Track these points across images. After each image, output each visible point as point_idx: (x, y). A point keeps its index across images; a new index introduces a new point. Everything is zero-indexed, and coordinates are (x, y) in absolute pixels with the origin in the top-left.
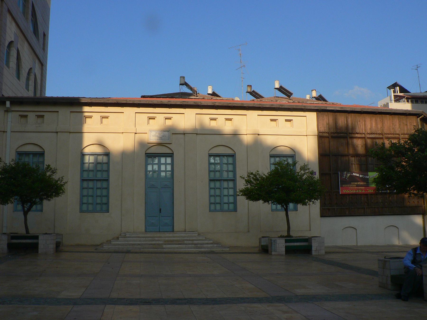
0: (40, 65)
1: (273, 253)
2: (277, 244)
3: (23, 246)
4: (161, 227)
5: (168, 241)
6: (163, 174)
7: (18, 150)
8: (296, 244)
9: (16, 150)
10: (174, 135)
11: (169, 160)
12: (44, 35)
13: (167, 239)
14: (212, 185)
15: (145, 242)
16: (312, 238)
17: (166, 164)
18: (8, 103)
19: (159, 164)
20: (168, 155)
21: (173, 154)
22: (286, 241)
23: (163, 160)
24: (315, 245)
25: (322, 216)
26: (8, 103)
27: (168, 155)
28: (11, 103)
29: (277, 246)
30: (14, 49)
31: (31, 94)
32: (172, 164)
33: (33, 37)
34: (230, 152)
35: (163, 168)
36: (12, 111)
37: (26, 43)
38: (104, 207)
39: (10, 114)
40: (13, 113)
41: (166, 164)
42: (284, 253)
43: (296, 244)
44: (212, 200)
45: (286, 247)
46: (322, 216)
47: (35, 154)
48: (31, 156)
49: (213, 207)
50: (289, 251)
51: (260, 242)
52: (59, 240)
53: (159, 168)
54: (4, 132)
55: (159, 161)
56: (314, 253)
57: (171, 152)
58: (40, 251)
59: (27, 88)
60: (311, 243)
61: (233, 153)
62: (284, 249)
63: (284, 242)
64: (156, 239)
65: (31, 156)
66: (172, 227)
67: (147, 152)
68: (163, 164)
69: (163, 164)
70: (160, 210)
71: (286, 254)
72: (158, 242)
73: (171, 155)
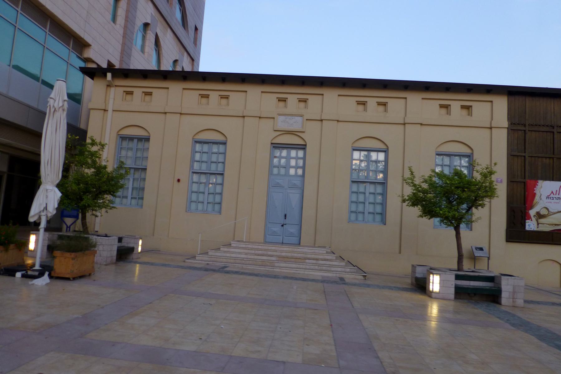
0: (191, 61)
4: (267, 236)
5: (284, 257)
6: (292, 172)
7: (121, 133)
9: (118, 132)
10: (308, 122)
11: (301, 153)
12: (196, 29)
13: (284, 254)
14: (355, 188)
15: (289, 255)
16: (503, 277)
17: (297, 158)
19: (288, 158)
20: (298, 147)
21: (306, 145)
22: (458, 277)
23: (293, 153)
24: (506, 286)
25: (507, 241)
26: (109, 75)
27: (298, 147)
28: (113, 77)
30: (151, 33)
32: (304, 158)
33: (181, 29)
34: (220, 138)
35: (293, 162)
36: (116, 86)
37: (169, 30)
38: (217, 207)
39: (113, 89)
40: (117, 88)
41: (297, 158)
42: (452, 296)
44: (353, 208)
46: (507, 241)
49: (353, 216)
51: (414, 271)
53: (288, 162)
55: (289, 154)
56: (504, 301)
57: (303, 143)
60: (500, 284)
65: (136, 141)
66: (299, 238)
67: (273, 142)
68: (293, 158)
69: (293, 158)
70: (285, 216)
71: (456, 298)
73: (303, 147)
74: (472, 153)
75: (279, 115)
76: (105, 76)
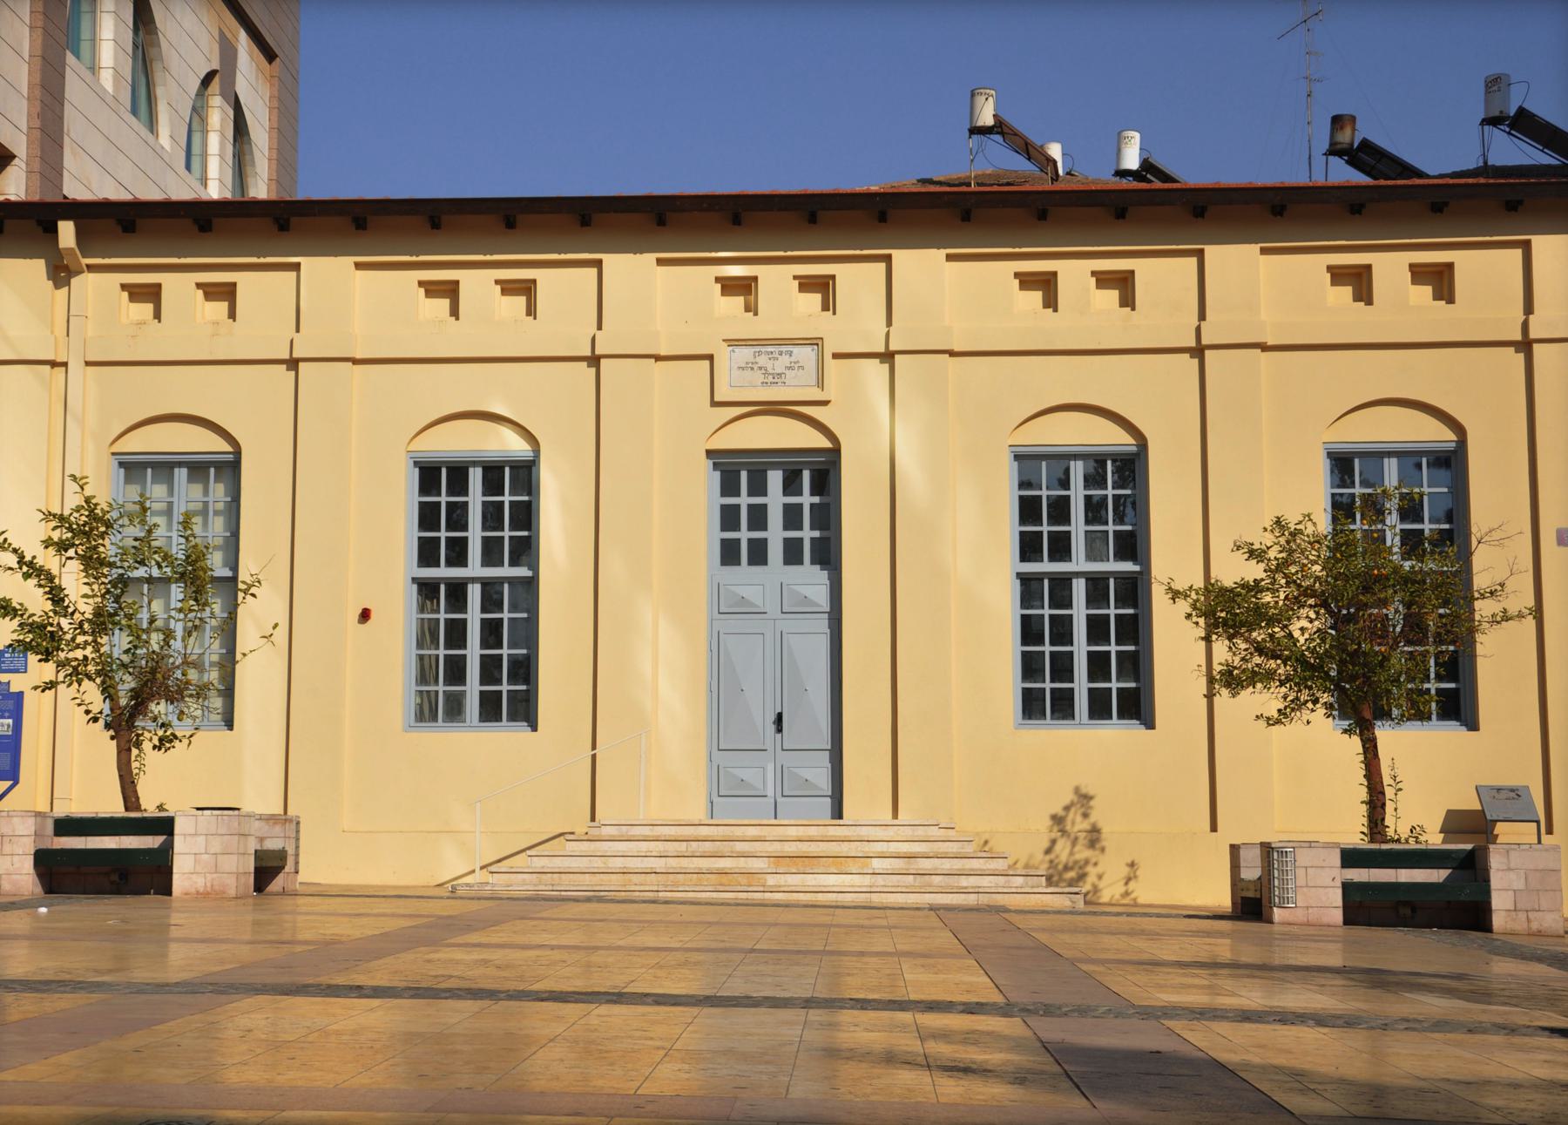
1: (1278, 914)
2: (1300, 872)
3: (107, 865)
4: (780, 800)
8: (1405, 876)
18: (67, 232)
26: (67, 232)
29: (1301, 881)
31: (216, 189)
43: (1405, 876)
45: (1348, 887)
47: (198, 468)
48: (181, 474)
50: (1362, 907)
52: (273, 845)
54: (53, 364)
56: (1498, 921)
58: (179, 883)
59: (192, 156)
61: (1448, 435)
62: (1337, 897)
63: (1338, 862)
64: (740, 847)
70: (779, 719)
72: (742, 863)
74: (1462, 442)
75: (733, 343)
76: (53, 231)
